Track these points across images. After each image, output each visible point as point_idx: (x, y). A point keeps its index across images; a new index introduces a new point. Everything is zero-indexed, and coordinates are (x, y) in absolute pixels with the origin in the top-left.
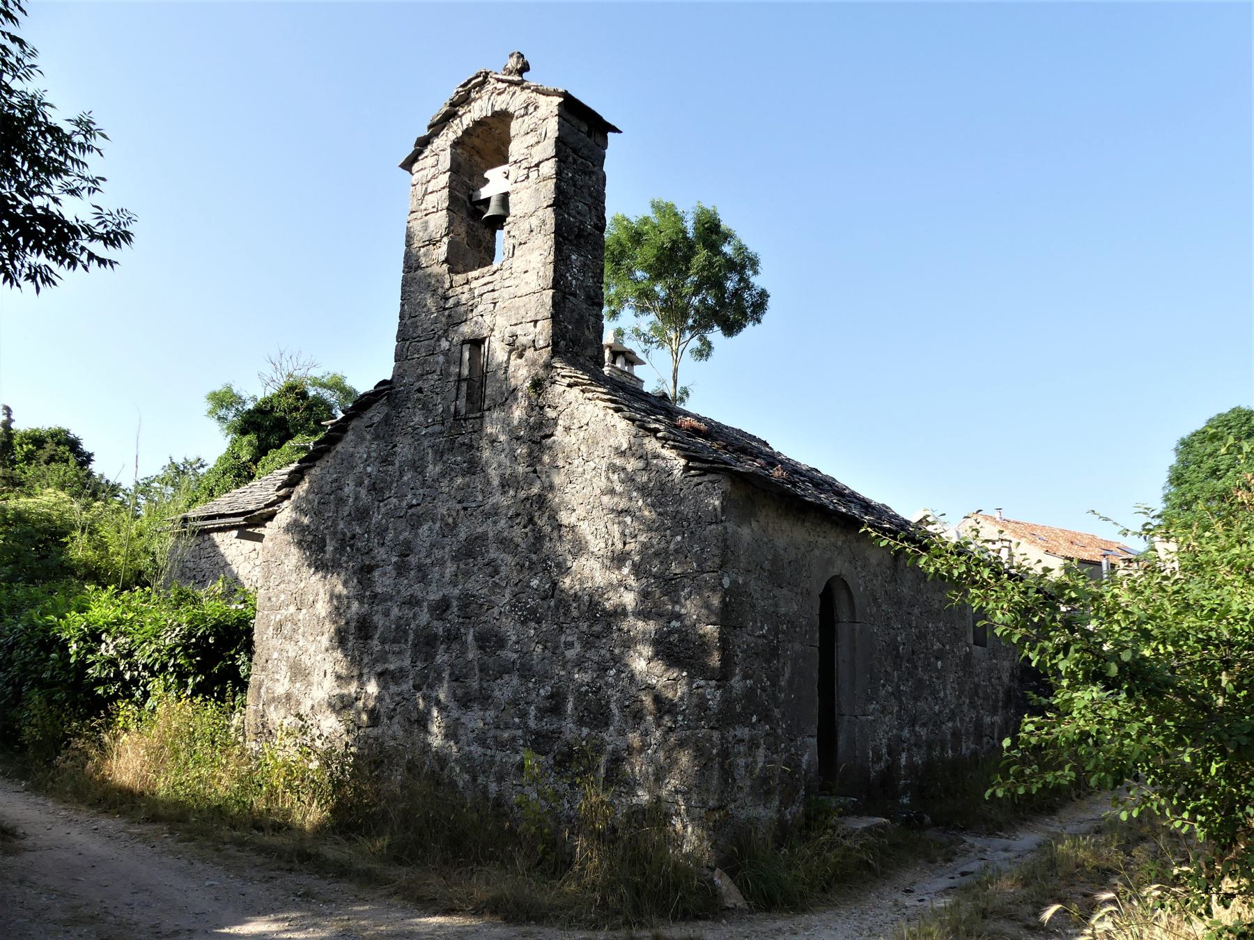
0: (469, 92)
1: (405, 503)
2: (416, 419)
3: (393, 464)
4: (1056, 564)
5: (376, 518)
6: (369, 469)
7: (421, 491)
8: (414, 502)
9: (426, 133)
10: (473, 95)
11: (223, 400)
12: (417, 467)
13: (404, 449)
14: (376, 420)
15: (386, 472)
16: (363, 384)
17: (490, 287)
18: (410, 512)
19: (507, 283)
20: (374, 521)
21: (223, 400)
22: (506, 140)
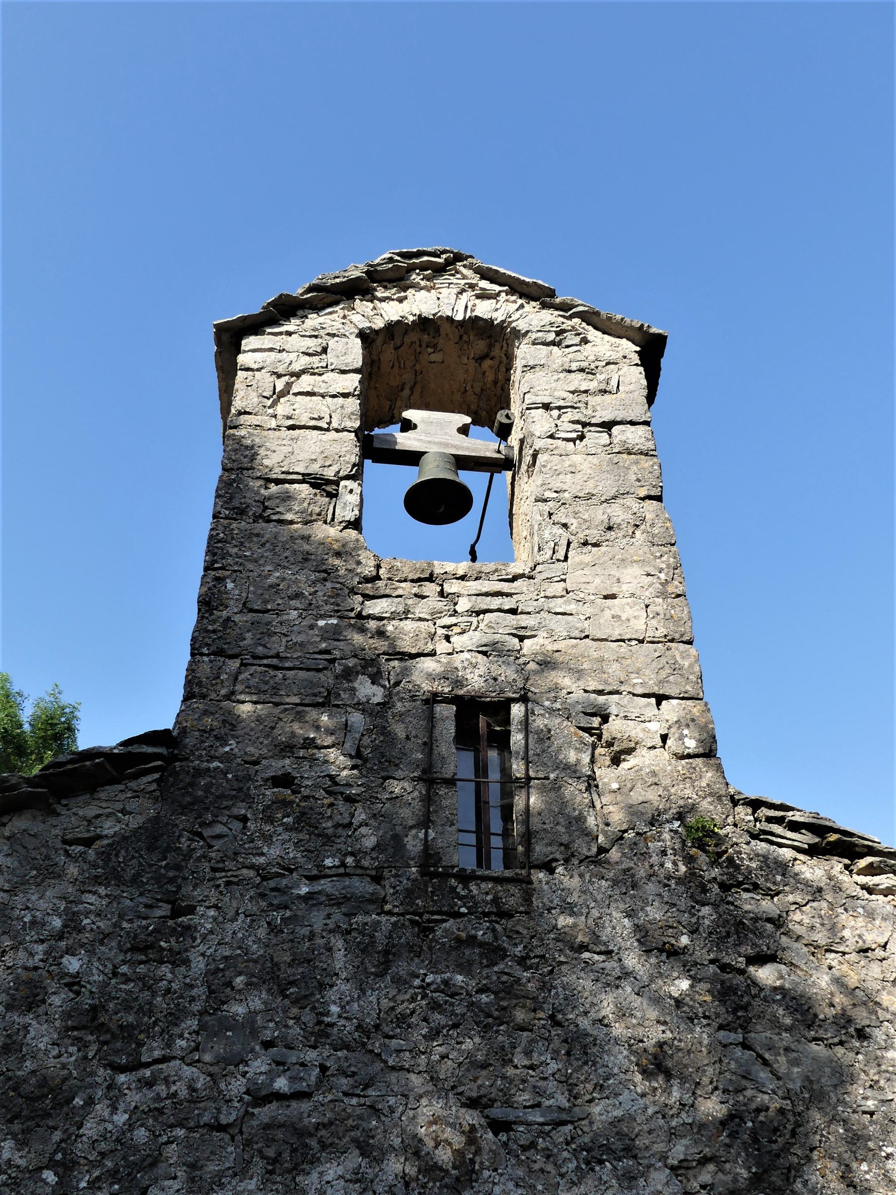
0: (411, 269)
1: (236, 1086)
2: (274, 852)
3: (178, 960)
4: (676, 1162)
5: (102, 1121)
6: (73, 964)
7: (311, 1055)
8: (281, 1084)
9: (297, 291)
10: (415, 277)
11: (57, 691)
12: (295, 982)
13: (223, 926)
14: (109, 828)
15: (147, 984)
16: (98, 732)
17: (508, 603)
18: (265, 1113)
19: (559, 605)
20: (90, 1129)
21: (57, 691)
22: (370, 371)
